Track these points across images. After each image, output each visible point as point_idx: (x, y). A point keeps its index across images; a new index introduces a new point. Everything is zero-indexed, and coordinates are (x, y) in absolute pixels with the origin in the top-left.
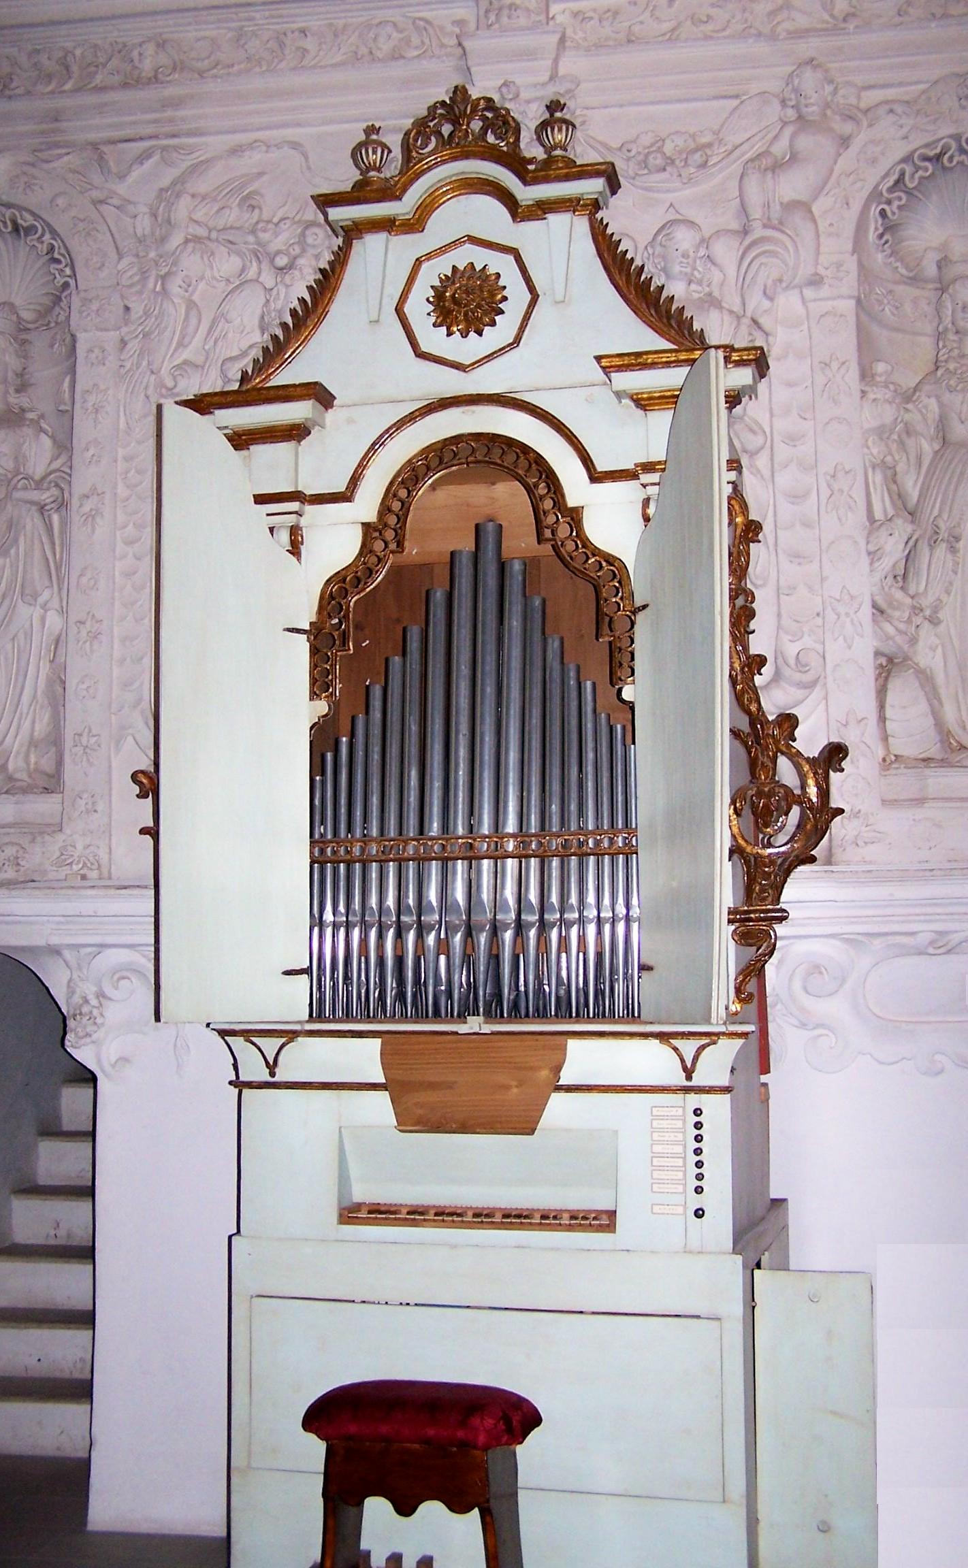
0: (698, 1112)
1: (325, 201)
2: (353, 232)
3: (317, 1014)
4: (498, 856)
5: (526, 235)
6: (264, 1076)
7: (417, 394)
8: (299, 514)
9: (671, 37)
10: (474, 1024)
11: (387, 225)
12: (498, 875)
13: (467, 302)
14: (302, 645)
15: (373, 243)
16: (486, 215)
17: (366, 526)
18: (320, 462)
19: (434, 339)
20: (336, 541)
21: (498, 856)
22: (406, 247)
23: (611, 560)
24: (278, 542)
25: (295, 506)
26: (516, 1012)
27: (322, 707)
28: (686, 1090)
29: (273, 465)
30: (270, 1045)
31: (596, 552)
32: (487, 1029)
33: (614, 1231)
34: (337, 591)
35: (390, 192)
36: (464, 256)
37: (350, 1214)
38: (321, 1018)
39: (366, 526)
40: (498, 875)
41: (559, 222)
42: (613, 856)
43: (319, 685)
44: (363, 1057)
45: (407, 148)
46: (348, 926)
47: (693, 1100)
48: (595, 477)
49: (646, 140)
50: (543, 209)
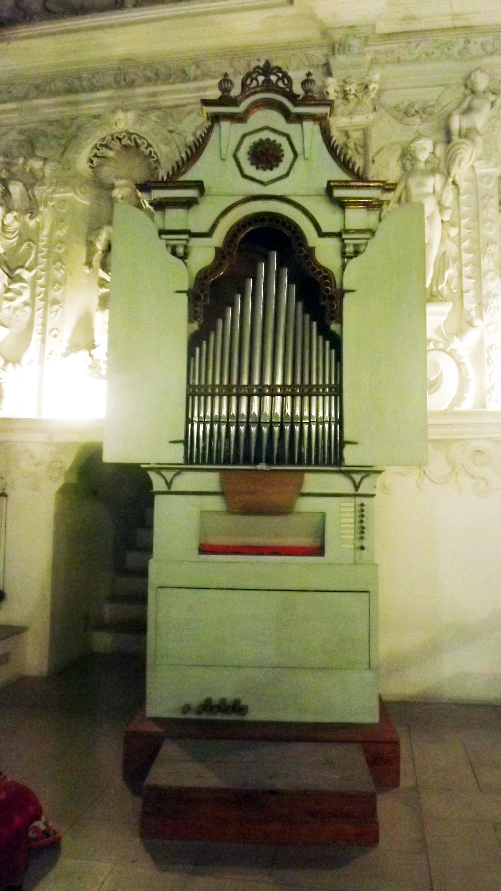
0: (362, 505)
1: (206, 102)
2: (215, 118)
3: (188, 459)
4: (273, 395)
5: (293, 129)
6: (164, 488)
7: (242, 192)
8: (187, 240)
9: (417, 60)
10: (262, 466)
11: (233, 118)
12: (272, 403)
13: (266, 155)
14: (184, 298)
15: (225, 125)
16: (275, 119)
17: (217, 249)
18: (199, 218)
19: (250, 170)
20: (203, 254)
21: (273, 395)
22: (239, 129)
23: (326, 270)
24: (4, 217)
25: (186, 237)
26: (280, 461)
27: (195, 326)
28: (355, 496)
29: (175, 218)
30: (169, 475)
31: (320, 266)
32: (268, 468)
33: (324, 556)
34: (202, 277)
35: (235, 102)
36: (265, 135)
37: (205, 549)
38: (191, 463)
39: (217, 249)
40: (272, 403)
41: (308, 125)
42: (324, 396)
43: (192, 317)
44: (210, 480)
45: (244, 84)
46: (205, 423)
47: (359, 500)
48: (321, 234)
49: (406, 104)
50: (299, 118)
